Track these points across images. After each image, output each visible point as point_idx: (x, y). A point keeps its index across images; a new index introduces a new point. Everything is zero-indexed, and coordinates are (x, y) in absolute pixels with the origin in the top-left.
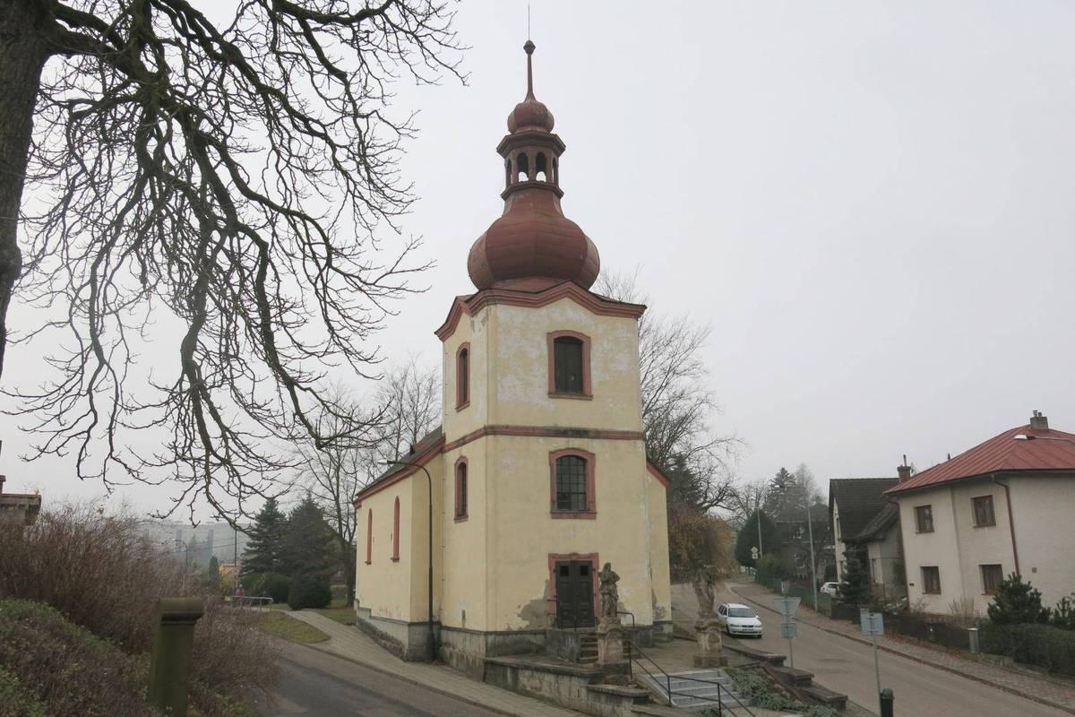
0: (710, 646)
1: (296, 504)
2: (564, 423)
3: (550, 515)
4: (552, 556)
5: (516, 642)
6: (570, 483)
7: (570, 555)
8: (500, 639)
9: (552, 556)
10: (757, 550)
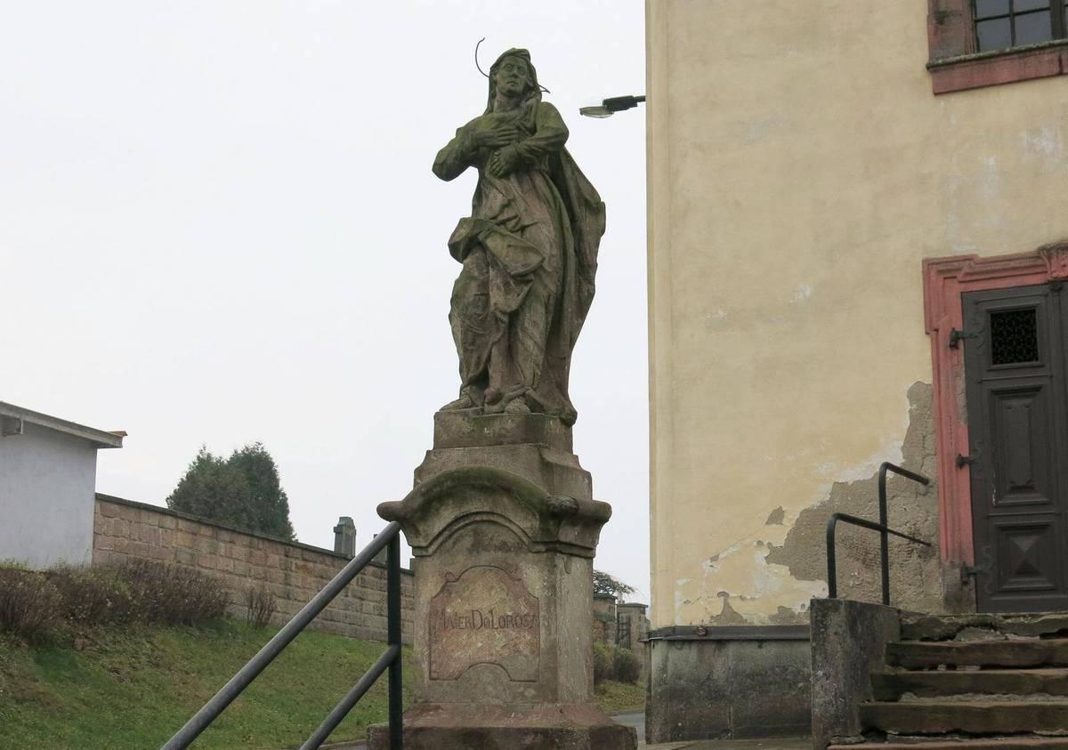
2: (993, 281)
3: (928, 82)
4: (940, 271)
5: (757, 680)
8: (686, 659)
9: (940, 271)
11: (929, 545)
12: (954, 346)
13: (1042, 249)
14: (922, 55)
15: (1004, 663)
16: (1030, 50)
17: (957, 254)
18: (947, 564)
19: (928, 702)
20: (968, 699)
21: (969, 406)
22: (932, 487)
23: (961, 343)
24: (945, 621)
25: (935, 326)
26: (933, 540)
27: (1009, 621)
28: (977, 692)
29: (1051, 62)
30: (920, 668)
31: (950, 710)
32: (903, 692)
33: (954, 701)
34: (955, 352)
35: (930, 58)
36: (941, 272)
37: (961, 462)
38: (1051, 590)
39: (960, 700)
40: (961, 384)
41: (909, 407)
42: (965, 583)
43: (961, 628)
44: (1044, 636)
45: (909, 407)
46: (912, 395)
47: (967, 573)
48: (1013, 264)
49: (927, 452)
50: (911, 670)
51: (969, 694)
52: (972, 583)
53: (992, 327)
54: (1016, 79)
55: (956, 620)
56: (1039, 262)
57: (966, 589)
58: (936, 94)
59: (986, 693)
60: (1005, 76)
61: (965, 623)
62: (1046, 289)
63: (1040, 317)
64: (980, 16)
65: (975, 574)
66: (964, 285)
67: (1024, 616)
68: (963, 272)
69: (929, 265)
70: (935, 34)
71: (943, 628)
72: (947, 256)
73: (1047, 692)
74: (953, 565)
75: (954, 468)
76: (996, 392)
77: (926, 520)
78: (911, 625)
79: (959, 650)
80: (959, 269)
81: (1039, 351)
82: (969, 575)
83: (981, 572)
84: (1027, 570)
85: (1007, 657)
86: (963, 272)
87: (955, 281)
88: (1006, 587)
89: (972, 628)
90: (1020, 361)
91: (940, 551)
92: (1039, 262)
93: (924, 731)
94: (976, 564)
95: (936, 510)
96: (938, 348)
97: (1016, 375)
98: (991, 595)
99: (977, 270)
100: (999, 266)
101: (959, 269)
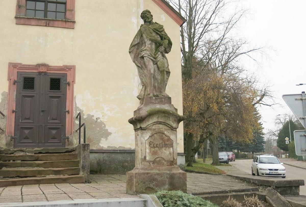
0: (154, 153)
1: (16, 75)
3: (15, 21)
4: (71, 68)
6: (56, 12)
7: (39, 65)
10: (288, 139)
11: (3, 131)
12: (14, 84)
13: (38, 64)
14: (13, 14)
15: (27, 160)
16: (40, 19)
17: (18, 62)
18: (7, 136)
19: (9, 169)
20: (19, 168)
21: (16, 98)
22: (5, 117)
23: (16, 83)
24: (12, 150)
25: (10, 78)
26: (4, 130)
27: (27, 150)
28: (22, 167)
29: (44, 23)
30: (6, 161)
31: (17, 171)
32: (3, 167)
33: (16, 169)
34: (14, 85)
35: (16, 15)
36: (13, 66)
37: (13, 112)
38: (32, 143)
39: (17, 169)
40: (15, 93)
41: (1, 97)
42: (12, 140)
43: (16, 151)
44: (35, 153)
45: (1, 97)
46: (3, 94)
47: (12, 138)
48: (31, 67)
49: (5, 108)
50: (4, 161)
51: (20, 167)
52: (13, 141)
53: (24, 80)
54: (36, 25)
55: (14, 149)
56: (37, 67)
57: (11, 142)
58: (16, 24)
59: (24, 167)
60: (33, 23)
61: (16, 150)
62: (38, 74)
63: (35, 80)
64: (27, 8)
65: (14, 138)
66: (18, 70)
67: (30, 149)
68: (18, 67)
69: (10, 64)
70: (18, 10)
71: (11, 151)
72: (15, 62)
73: (39, 167)
74: (9, 136)
75: (11, 114)
76: (24, 96)
77: (3, 125)
78: (3, 150)
79: (16, 157)
80: (17, 66)
81: (34, 87)
82: (13, 138)
83: (15, 138)
84: (27, 138)
85: (28, 158)
86: (18, 67)
87: (16, 69)
88: (49, 142)
89: (18, 151)
90: (29, 89)
91: (6, 133)
92: (37, 67)
93: (10, 177)
94: (14, 136)
95: (6, 123)
96: (10, 84)
97: (29, 92)
98: (17, 144)
99: (22, 67)
100: (28, 67)
101: (17, 66)
